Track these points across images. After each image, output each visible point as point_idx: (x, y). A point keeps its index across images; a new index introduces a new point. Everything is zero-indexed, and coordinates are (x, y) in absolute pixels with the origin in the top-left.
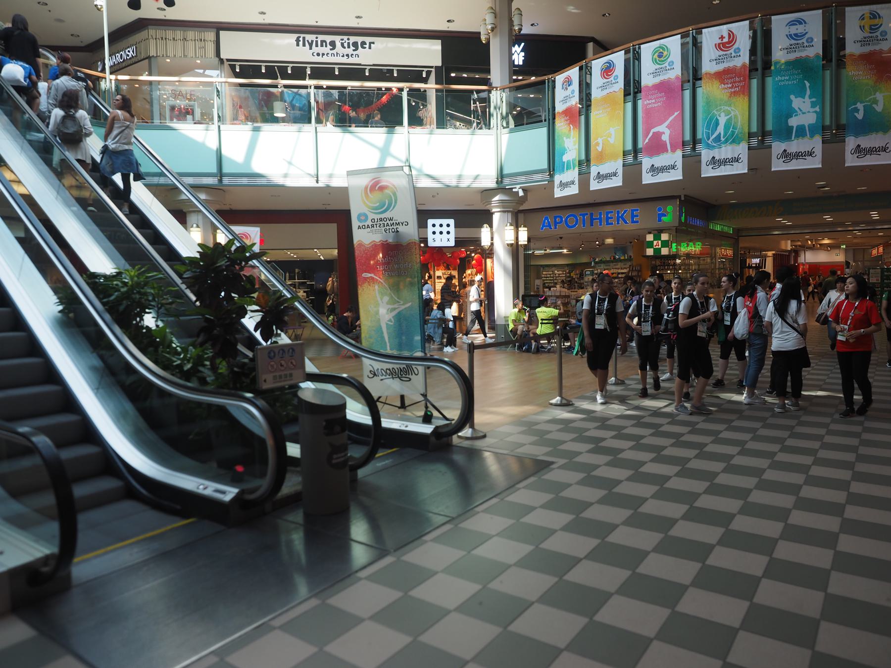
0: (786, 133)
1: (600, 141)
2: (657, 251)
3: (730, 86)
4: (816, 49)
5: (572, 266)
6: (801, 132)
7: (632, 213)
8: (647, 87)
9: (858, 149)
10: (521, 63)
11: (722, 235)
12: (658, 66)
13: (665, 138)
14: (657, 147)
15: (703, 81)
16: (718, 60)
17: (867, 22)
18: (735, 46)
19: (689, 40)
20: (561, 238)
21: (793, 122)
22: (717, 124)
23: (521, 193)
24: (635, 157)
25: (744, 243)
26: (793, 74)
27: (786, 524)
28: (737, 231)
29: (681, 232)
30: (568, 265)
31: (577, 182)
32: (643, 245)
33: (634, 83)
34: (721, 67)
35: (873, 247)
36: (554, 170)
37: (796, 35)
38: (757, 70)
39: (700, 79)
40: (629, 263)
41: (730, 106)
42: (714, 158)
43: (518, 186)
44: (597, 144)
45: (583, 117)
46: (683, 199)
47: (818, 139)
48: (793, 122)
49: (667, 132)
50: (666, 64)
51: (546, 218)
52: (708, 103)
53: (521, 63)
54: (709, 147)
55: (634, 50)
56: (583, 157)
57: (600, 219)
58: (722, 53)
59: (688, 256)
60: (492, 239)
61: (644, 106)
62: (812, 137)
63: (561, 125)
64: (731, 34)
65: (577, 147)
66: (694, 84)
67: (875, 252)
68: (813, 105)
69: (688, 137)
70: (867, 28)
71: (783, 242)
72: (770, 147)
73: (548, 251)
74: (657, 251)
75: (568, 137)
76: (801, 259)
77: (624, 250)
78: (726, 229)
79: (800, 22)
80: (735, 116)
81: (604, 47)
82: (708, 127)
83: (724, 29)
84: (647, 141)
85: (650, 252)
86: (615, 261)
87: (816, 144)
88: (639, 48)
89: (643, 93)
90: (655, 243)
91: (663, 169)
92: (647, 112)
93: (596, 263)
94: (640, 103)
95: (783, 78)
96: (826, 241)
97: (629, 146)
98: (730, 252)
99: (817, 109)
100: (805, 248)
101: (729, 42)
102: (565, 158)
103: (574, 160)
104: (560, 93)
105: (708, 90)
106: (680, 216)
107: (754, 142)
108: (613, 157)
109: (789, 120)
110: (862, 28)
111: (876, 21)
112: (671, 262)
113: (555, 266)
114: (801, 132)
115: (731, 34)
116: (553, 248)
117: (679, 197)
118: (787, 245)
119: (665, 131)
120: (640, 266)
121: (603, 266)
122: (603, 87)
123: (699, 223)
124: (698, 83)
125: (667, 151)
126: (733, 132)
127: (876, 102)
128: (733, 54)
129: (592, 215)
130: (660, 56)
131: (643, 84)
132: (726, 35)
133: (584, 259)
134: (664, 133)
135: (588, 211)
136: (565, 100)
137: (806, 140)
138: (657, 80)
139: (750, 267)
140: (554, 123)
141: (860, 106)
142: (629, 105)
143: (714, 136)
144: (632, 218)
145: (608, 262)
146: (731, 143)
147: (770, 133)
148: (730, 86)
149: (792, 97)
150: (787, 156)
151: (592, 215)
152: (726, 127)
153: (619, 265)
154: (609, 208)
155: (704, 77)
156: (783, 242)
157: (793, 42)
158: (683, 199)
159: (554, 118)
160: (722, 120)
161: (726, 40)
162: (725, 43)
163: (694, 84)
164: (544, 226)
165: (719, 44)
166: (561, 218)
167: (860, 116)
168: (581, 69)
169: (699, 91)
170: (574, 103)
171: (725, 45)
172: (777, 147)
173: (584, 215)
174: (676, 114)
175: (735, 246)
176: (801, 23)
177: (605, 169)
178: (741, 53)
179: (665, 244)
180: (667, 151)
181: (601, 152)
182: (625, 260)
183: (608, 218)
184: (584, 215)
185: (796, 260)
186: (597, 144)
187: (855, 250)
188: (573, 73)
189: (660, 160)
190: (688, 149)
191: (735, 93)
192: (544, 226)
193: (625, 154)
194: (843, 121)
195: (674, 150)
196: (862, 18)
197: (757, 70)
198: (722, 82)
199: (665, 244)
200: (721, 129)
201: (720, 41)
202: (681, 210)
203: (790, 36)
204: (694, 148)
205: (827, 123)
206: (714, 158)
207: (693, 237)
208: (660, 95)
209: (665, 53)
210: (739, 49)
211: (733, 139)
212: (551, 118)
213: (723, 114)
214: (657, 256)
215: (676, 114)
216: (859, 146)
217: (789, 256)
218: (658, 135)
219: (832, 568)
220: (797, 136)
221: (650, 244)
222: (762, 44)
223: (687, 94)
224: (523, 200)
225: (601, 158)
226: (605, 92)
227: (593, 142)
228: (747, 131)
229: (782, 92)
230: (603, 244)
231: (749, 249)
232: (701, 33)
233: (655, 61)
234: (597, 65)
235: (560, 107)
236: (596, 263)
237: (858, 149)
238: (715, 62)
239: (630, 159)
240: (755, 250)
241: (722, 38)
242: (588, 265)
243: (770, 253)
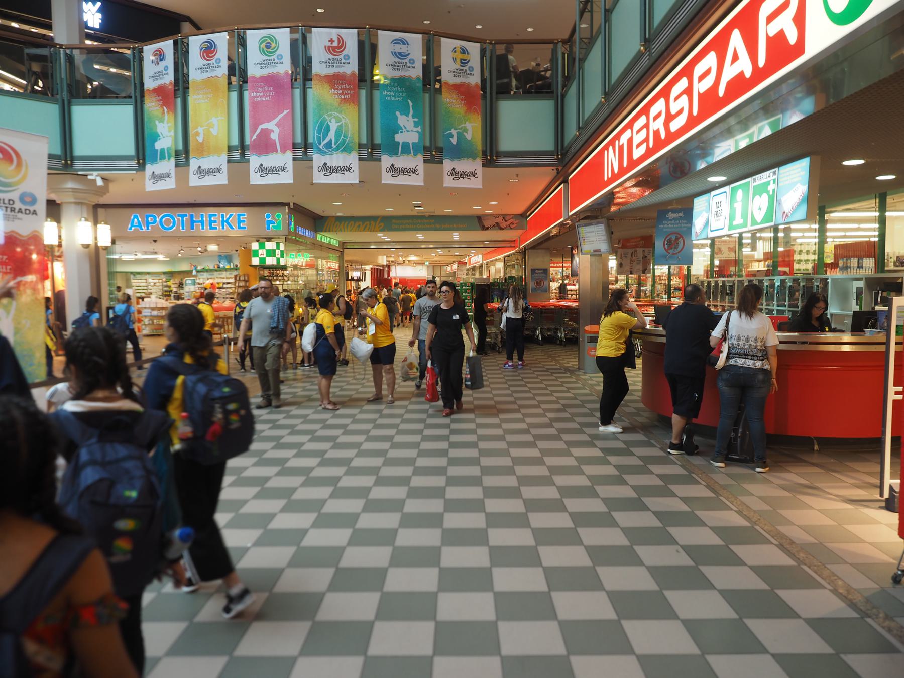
0: (393, 148)
1: (200, 130)
2: (262, 260)
3: (340, 92)
4: (416, 72)
5: (171, 274)
6: (406, 149)
7: (239, 218)
8: (253, 77)
9: (392, 168)
10: (97, 26)
11: (329, 248)
12: (266, 58)
13: (275, 136)
14: (265, 146)
15: (313, 82)
16: (329, 63)
17: (459, 56)
18: (345, 52)
19: (298, 36)
20: (155, 241)
21: (399, 138)
22: (328, 129)
23: (100, 182)
24: (243, 154)
25: (349, 255)
26: (398, 92)
27: (440, 568)
28: (343, 245)
29: (292, 240)
30: (164, 273)
31: (173, 174)
32: (248, 253)
33: (240, 72)
34: (331, 71)
35: (448, 264)
36: (144, 159)
37: (400, 53)
38: (365, 81)
39: (311, 80)
40: (235, 273)
41: (340, 113)
42: (325, 164)
43: (95, 173)
44: (197, 134)
45: (179, 101)
46: (292, 206)
47: (289, 155)
48: (399, 138)
49: (277, 130)
50: (275, 57)
51: (136, 217)
52: (321, 107)
53: (97, 26)
54: (321, 152)
55: (239, 35)
56: (180, 147)
57: (202, 222)
58: (331, 57)
59: (295, 267)
60: (60, 237)
61: (252, 99)
62: (415, 155)
63: (151, 105)
64: (340, 39)
65: (172, 133)
66: (304, 85)
67: (449, 269)
68: (416, 124)
69: (299, 139)
70: (458, 61)
71: (380, 257)
72: (380, 160)
73: (140, 256)
74: (262, 260)
75: (161, 121)
76: (392, 274)
77: (229, 259)
78: (332, 242)
79: (403, 42)
80: (346, 125)
81: (198, 28)
82: (319, 131)
83: (334, 32)
84: (254, 137)
85: (255, 261)
86: (219, 269)
87: (285, 159)
88: (245, 33)
89: (249, 85)
90: (260, 251)
91: (273, 170)
92: (255, 105)
93: (198, 271)
94: (246, 94)
95: (389, 94)
96: (413, 258)
97: (235, 141)
98: (335, 265)
99: (419, 129)
100: (395, 263)
101: (339, 47)
102: (158, 145)
103: (169, 149)
104: (149, 69)
105: (318, 93)
106: (289, 224)
107: (365, 153)
108: (217, 151)
109: (396, 136)
110: (454, 60)
111: (465, 56)
112: (280, 273)
113: (148, 273)
114: (406, 149)
115: (340, 39)
116: (145, 253)
117: (288, 204)
118: (383, 260)
119: (273, 128)
120: (248, 276)
121: (206, 275)
122: (203, 69)
123: (307, 233)
124: (308, 83)
125: (277, 151)
126: (344, 141)
127: (466, 130)
128: (343, 61)
129: (192, 217)
130: (268, 47)
131: (249, 73)
132: (335, 39)
133: (185, 267)
134: (273, 131)
135: (188, 212)
136: (155, 77)
137: (411, 156)
138: (265, 72)
139: (352, 279)
140: (142, 102)
141: (454, 132)
142: (234, 95)
143: (325, 142)
144: (239, 224)
145: (211, 271)
146: (342, 151)
147: (378, 147)
148: (340, 92)
149: (398, 113)
150: (327, 169)
151: (192, 217)
152: (338, 133)
153: (224, 274)
154: (212, 211)
155: (314, 79)
156: (380, 257)
157: (397, 60)
158: (292, 206)
159: (142, 96)
160: (334, 126)
161: (335, 44)
162: (331, 47)
163: (304, 85)
164: (132, 226)
165: (329, 47)
166: (155, 218)
167: (454, 141)
168: (176, 43)
169: (310, 92)
170: (414, 76)
171: (336, 48)
172: (386, 161)
173: (182, 217)
174: (286, 112)
175: (341, 258)
176: (404, 44)
177: (207, 163)
178: (350, 61)
179: (271, 253)
180: (277, 151)
181: (202, 144)
182: (230, 269)
183: (211, 222)
184: (182, 217)
185: (389, 275)
186: (197, 134)
187: (434, 266)
188: (167, 45)
189: (270, 160)
190: (300, 153)
191: (344, 101)
192: (132, 226)
193: (230, 149)
194: (440, 144)
195: (284, 151)
196: (454, 50)
197: (365, 81)
198: (333, 87)
199: (271, 253)
200: (332, 135)
201: (329, 44)
202: (290, 219)
203: (394, 54)
204: (305, 152)
205: (428, 144)
206: (325, 164)
207: (301, 247)
208: (267, 89)
209: (273, 45)
210: (348, 56)
211: (347, 149)
212: (138, 95)
213: (333, 120)
214: (263, 267)
215: (286, 112)
216: (454, 169)
217: (383, 270)
218: (266, 133)
219: (498, 619)
220: (403, 152)
221: (256, 253)
222: (368, 54)
223: (298, 93)
224: (103, 191)
225: (203, 150)
226: (206, 75)
227: (192, 131)
228: (357, 141)
229: (389, 108)
230: (206, 250)
231: (352, 262)
232: (311, 32)
233: (262, 51)
234: (196, 42)
235: (149, 84)
236: (198, 271)
237: (392, 168)
238: (325, 65)
239: (236, 155)
240: (356, 262)
241: (332, 41)
242: (188, 273)
243: (368, 267)
